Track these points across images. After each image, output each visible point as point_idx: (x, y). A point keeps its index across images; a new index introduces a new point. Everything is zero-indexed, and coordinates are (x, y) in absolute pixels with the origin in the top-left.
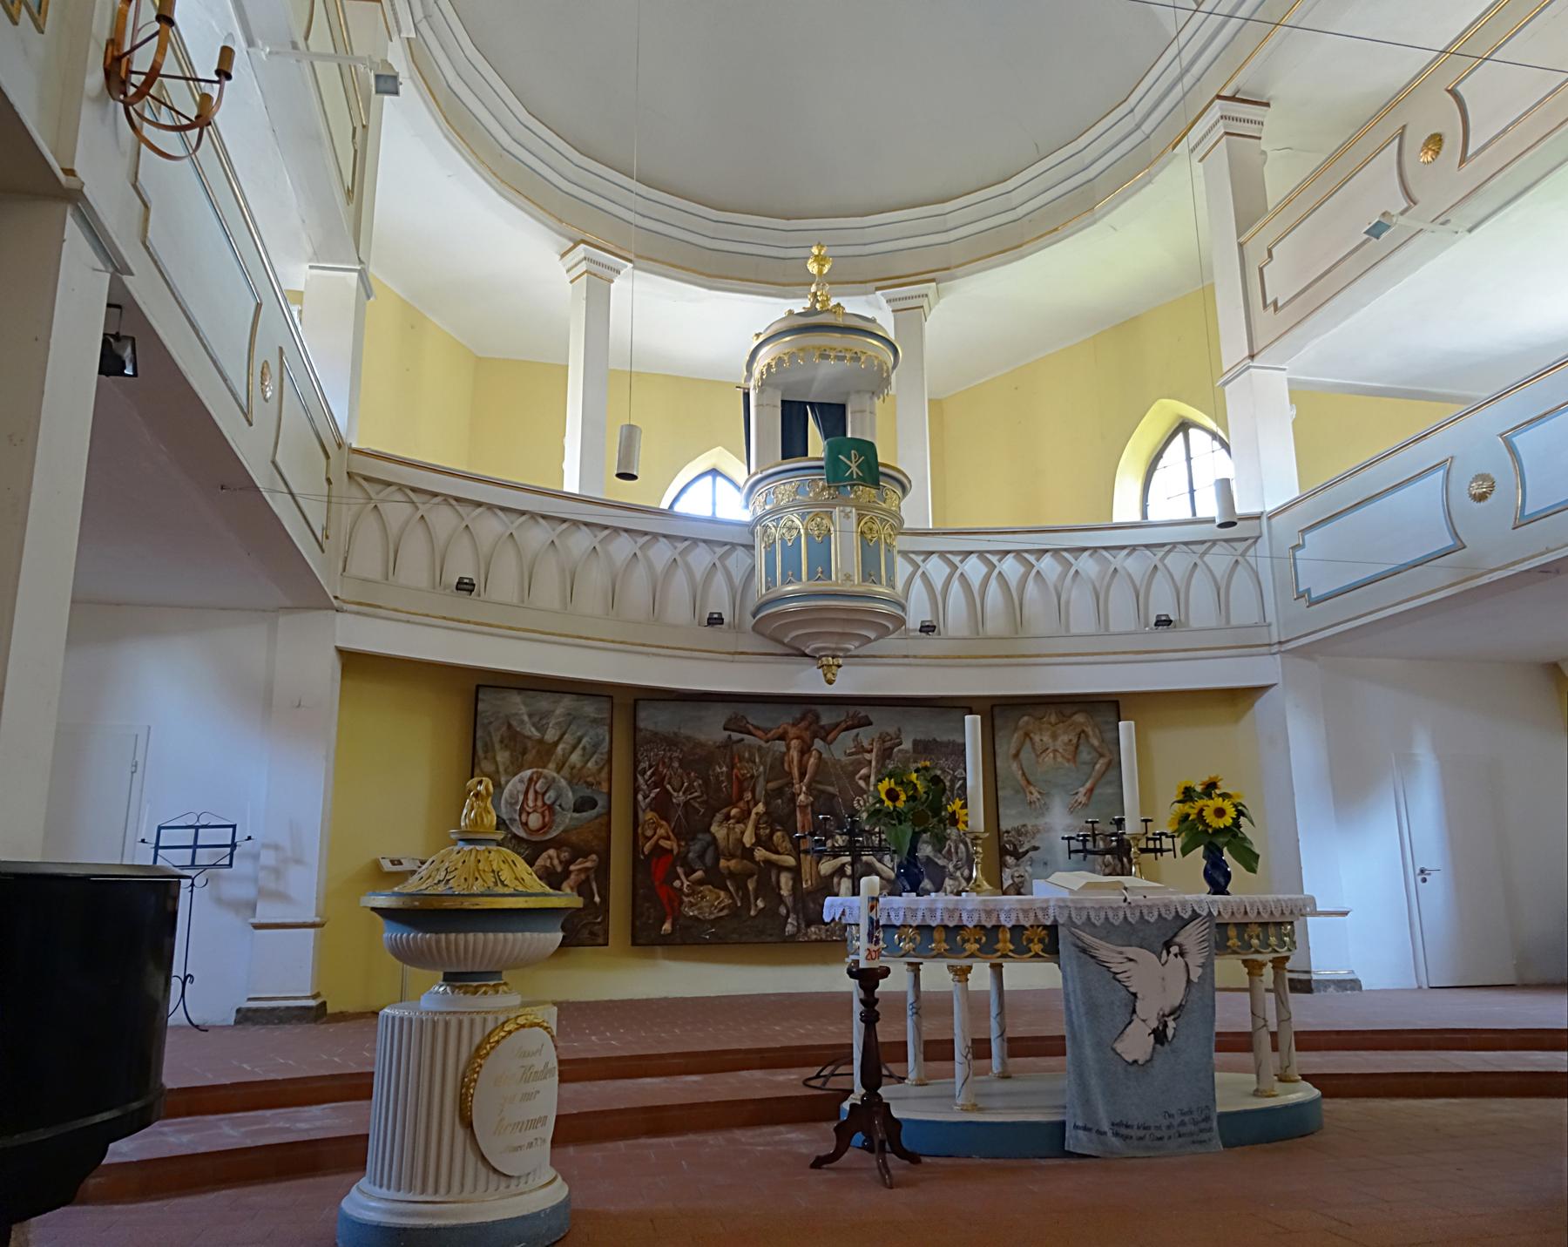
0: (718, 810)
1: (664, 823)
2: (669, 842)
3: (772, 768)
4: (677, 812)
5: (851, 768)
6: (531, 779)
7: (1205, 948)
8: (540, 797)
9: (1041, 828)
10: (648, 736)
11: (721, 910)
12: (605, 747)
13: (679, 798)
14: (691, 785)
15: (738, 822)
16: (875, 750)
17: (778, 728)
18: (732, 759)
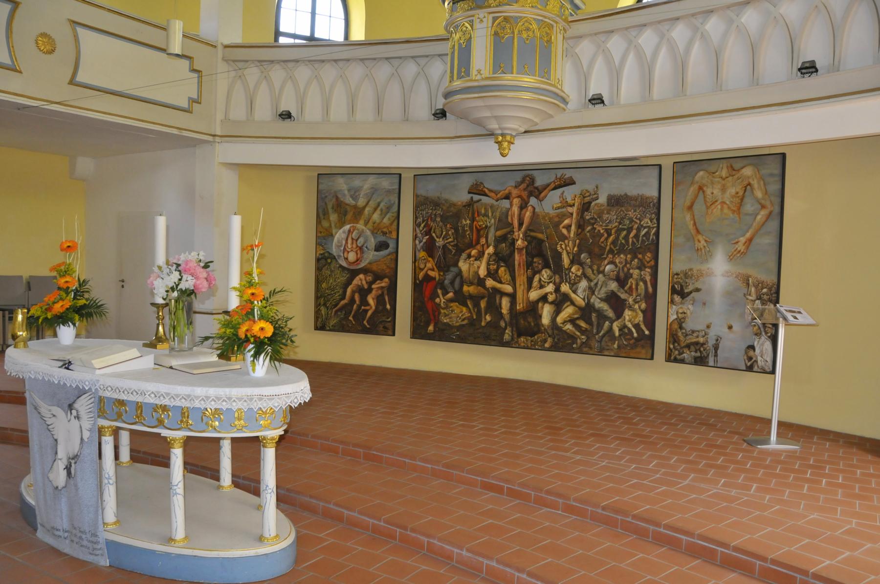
0: (464, 251)
1: (430, 259)
2: (433, 273)
3: (500, 220)
4: (439, 252)
5: (556, 219)
6: (349, 231)
7: (92, 417)
8: (355, 241)
9: (704, 272)
10: (422, 200)
11: (463, 320)
12: (395, 209)
13: (440, 242)
14: (447, 234)
15: (476, 260)
16: (576, 204)
17: (505, 190)
18: (473, 214)
